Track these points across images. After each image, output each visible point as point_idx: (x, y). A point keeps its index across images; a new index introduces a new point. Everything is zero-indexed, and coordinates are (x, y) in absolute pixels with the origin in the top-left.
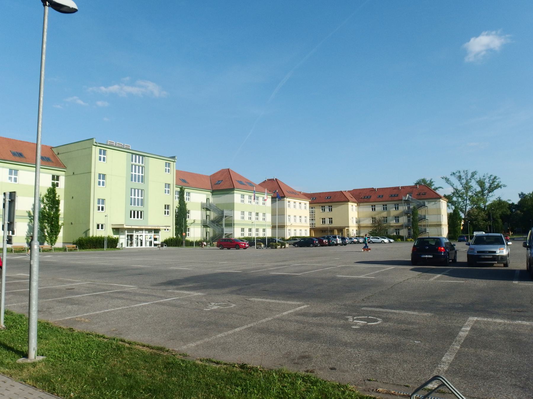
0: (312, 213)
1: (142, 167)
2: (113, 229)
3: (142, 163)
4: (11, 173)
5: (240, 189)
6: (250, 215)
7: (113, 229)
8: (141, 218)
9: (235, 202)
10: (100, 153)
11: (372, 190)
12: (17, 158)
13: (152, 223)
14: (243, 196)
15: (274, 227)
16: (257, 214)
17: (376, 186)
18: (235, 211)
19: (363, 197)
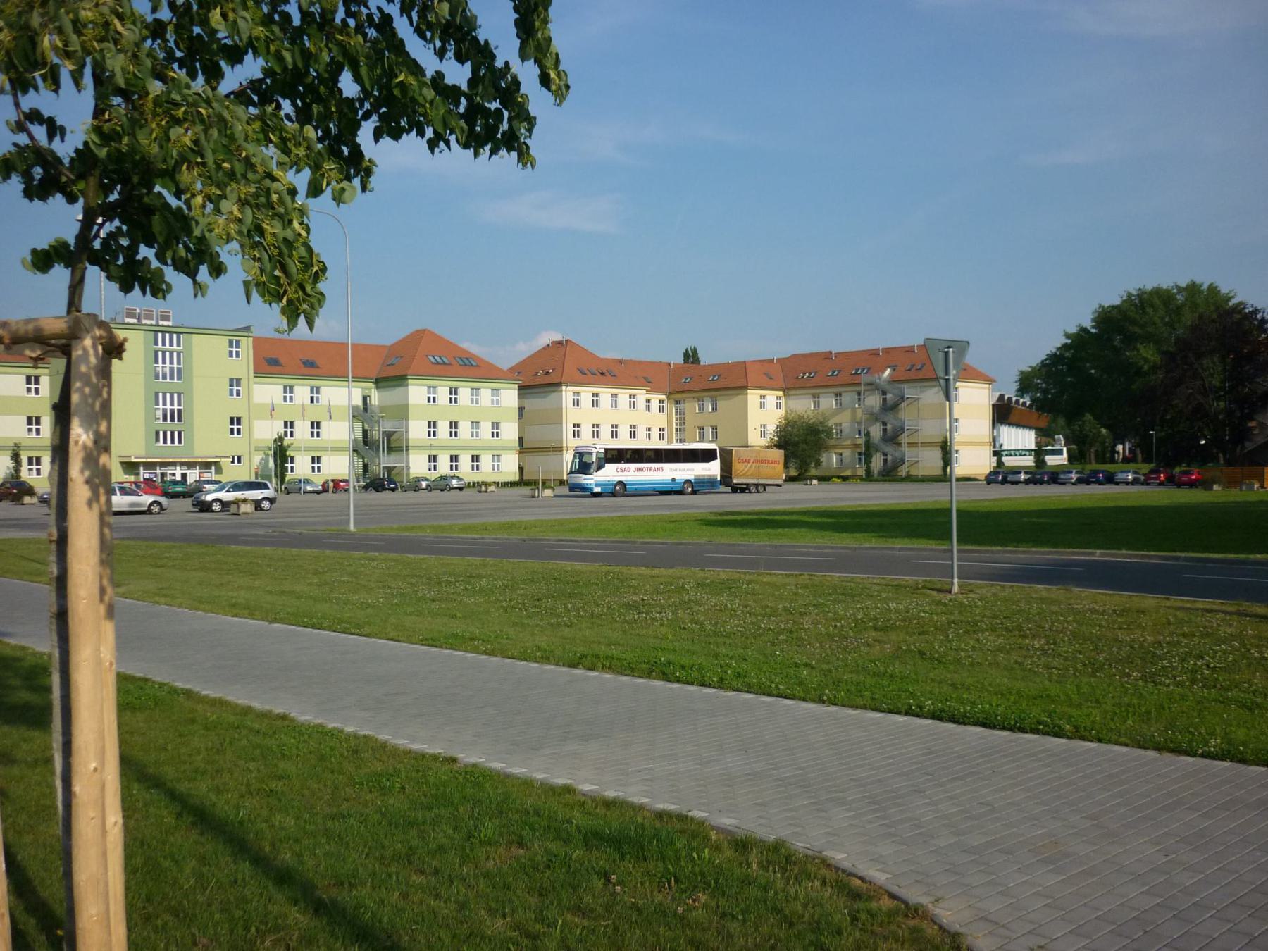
0: (681, 412)
1: (179, 353)
2: (122, 463)
3: (178, 345)
4: (28, 382)
5: (420, 375)
6: (601, 417)
7: (122, 463)
8: (180, 442)
9: (411, 402)
10: (231, 346)
11: (827, 356)
12: (307, 371)
13: (202, 451)
14: (454, 391)
15: (524, 448)
16: (454, 425)
17: (836, 349)
18: (411, 423)
19: (794, 374)
